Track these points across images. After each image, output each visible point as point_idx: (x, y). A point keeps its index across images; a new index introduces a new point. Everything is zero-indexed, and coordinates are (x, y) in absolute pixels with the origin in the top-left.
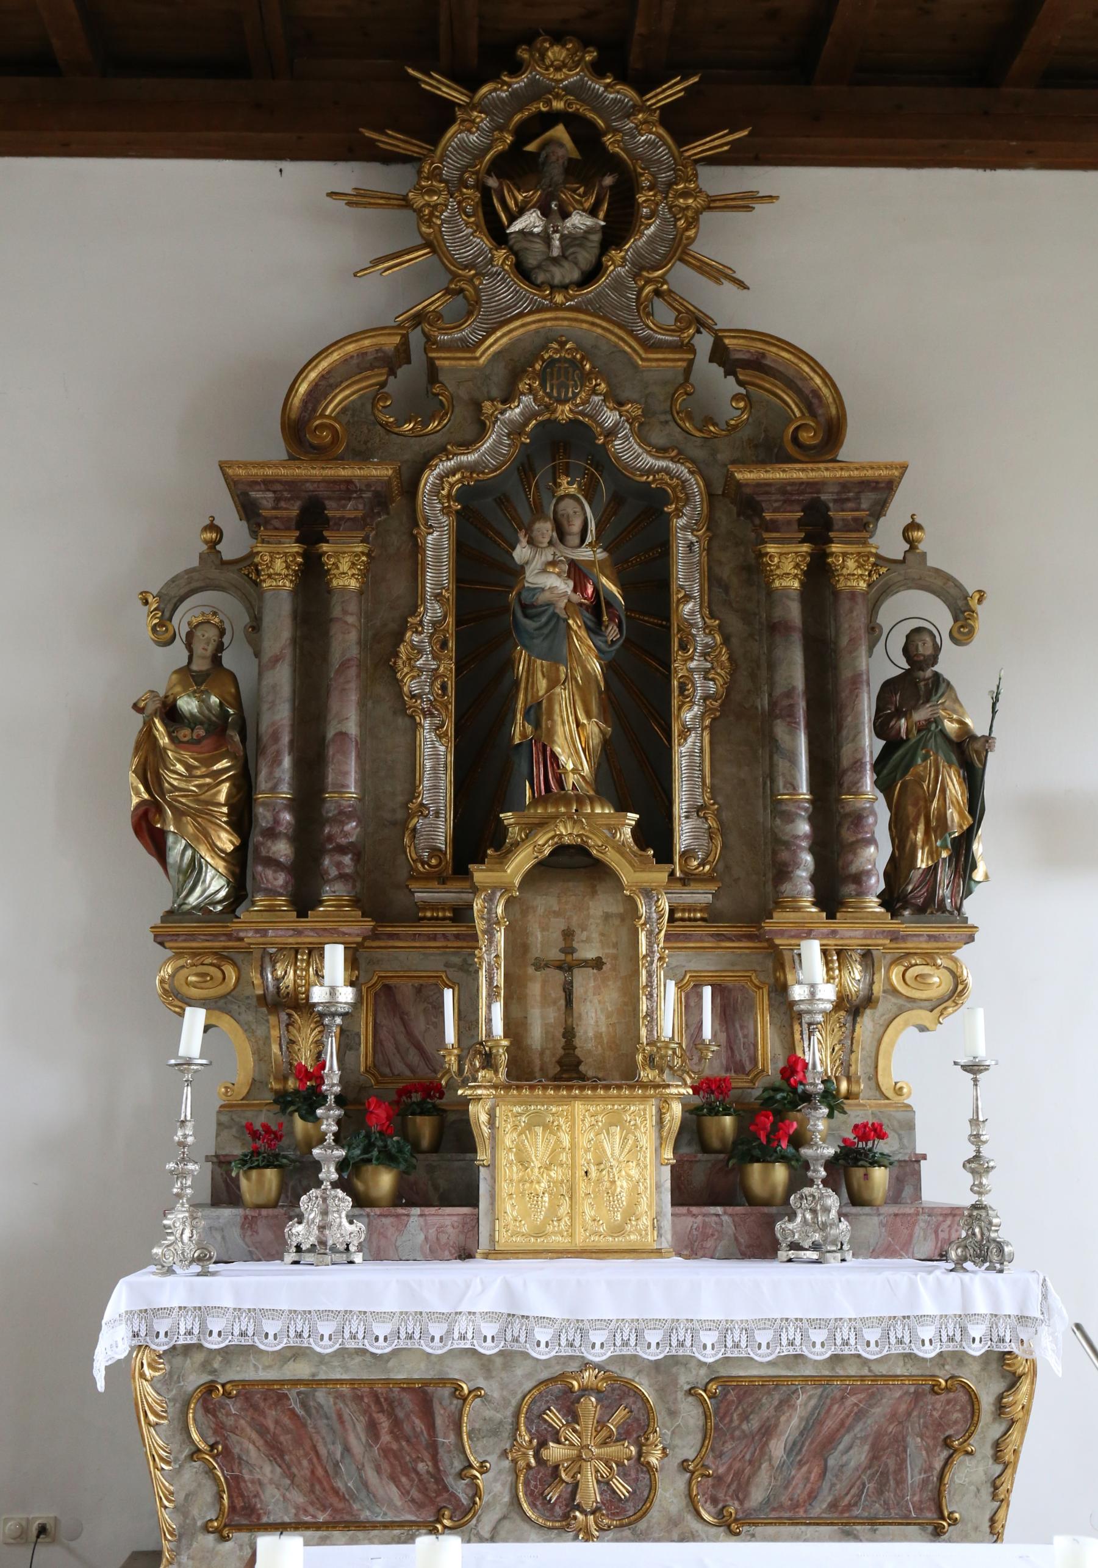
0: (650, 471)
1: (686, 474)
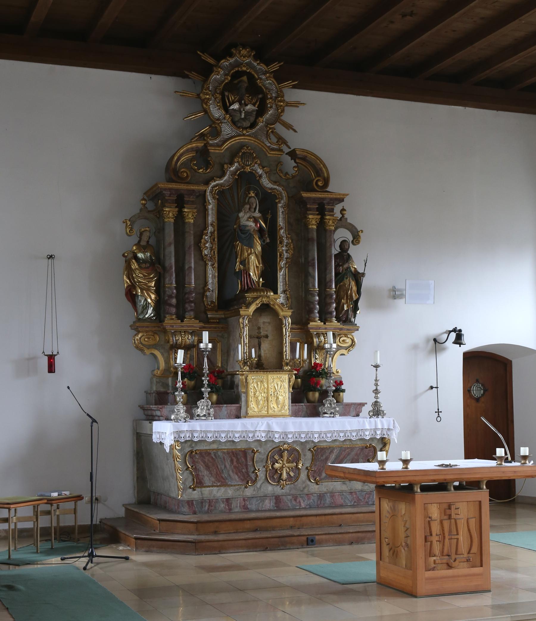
0: (271, 189)
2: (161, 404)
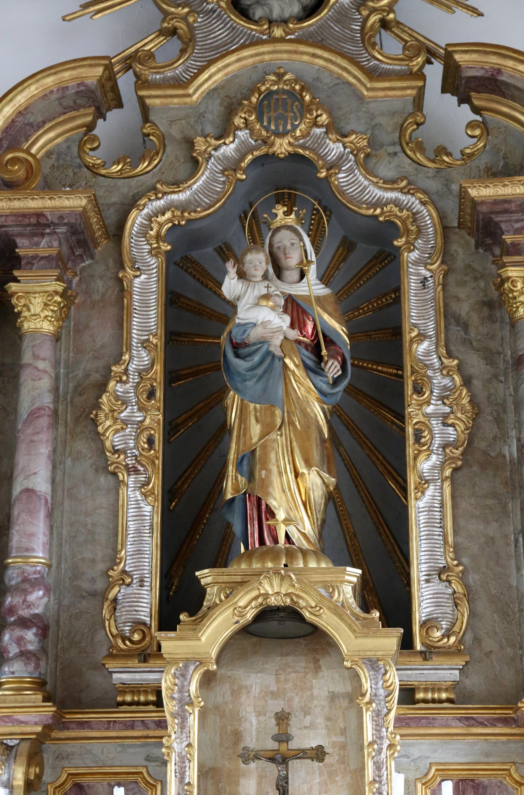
1: (417, 206)
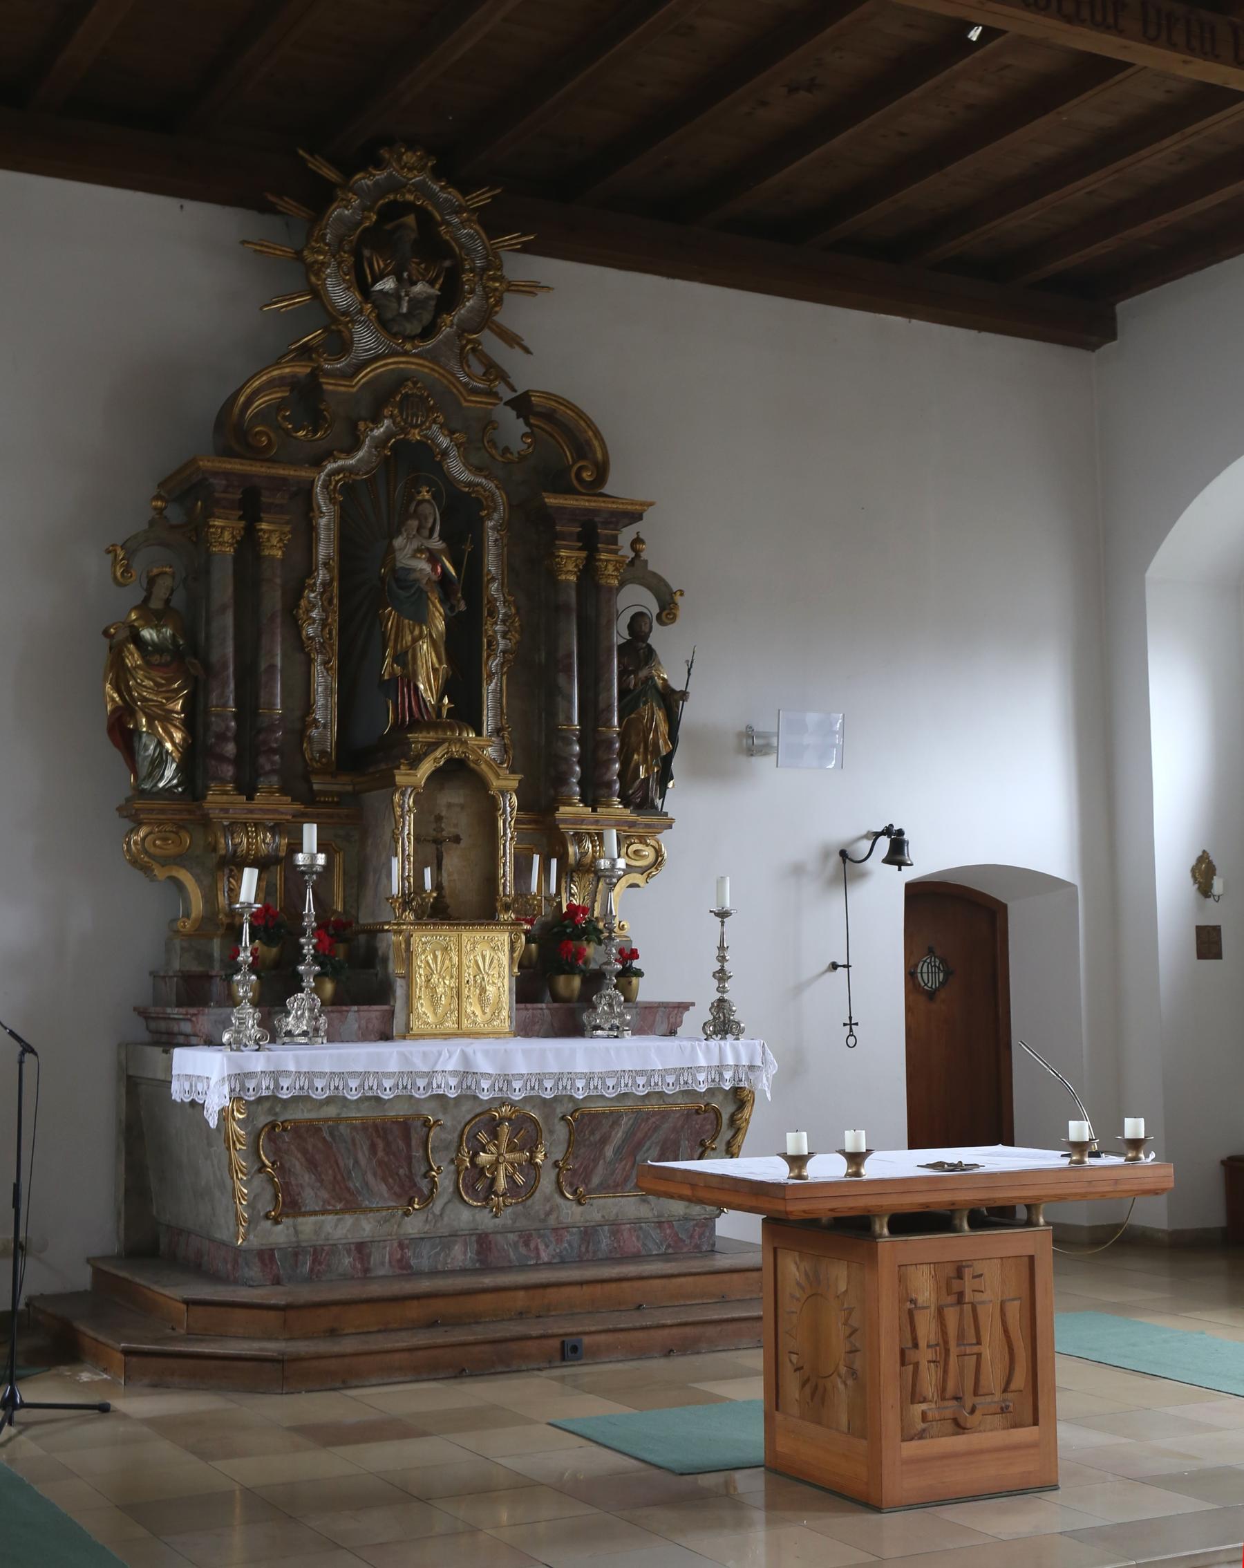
2: (191, 1004)
